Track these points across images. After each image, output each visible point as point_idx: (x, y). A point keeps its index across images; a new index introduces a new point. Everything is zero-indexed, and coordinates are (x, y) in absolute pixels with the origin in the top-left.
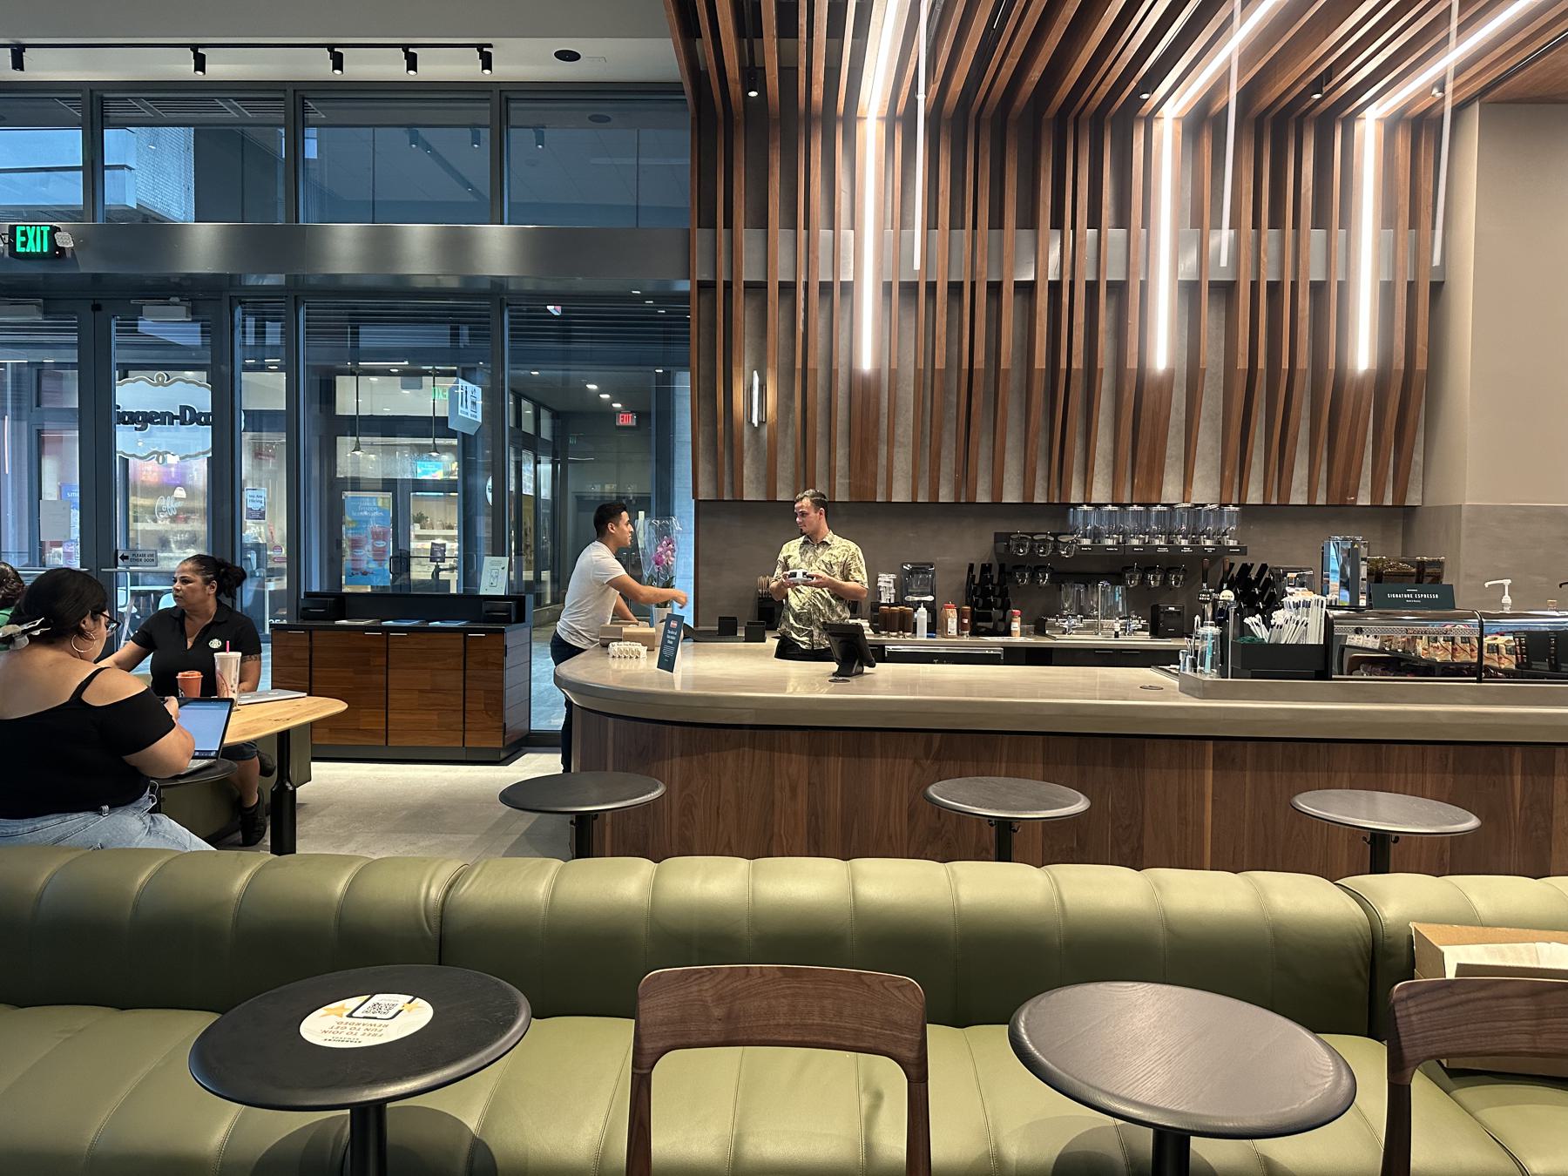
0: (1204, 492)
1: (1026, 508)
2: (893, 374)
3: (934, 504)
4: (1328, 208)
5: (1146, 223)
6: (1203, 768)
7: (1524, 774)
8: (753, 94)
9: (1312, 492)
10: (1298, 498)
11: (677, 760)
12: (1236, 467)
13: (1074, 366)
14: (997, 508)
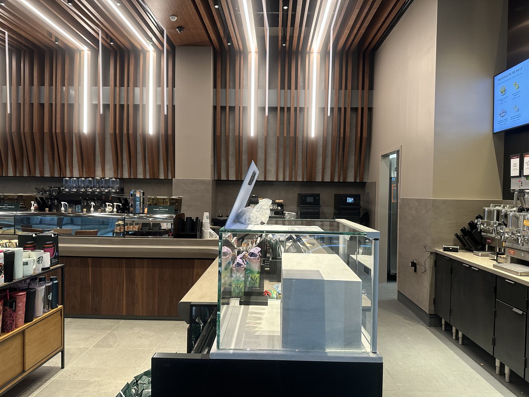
0: (109, 174)
1: (52, 179)
2: (266, 139)
3: (228, 180)
4: (138, 81)
5: (308, 89)
6: (89, 267)
7: (92, 267)
8: (229, 44)
9: (145, 174)
10: (140, 176)
11: (145, 269)
12: (118, 165)
13: (130, 132)
14: (42, 179)
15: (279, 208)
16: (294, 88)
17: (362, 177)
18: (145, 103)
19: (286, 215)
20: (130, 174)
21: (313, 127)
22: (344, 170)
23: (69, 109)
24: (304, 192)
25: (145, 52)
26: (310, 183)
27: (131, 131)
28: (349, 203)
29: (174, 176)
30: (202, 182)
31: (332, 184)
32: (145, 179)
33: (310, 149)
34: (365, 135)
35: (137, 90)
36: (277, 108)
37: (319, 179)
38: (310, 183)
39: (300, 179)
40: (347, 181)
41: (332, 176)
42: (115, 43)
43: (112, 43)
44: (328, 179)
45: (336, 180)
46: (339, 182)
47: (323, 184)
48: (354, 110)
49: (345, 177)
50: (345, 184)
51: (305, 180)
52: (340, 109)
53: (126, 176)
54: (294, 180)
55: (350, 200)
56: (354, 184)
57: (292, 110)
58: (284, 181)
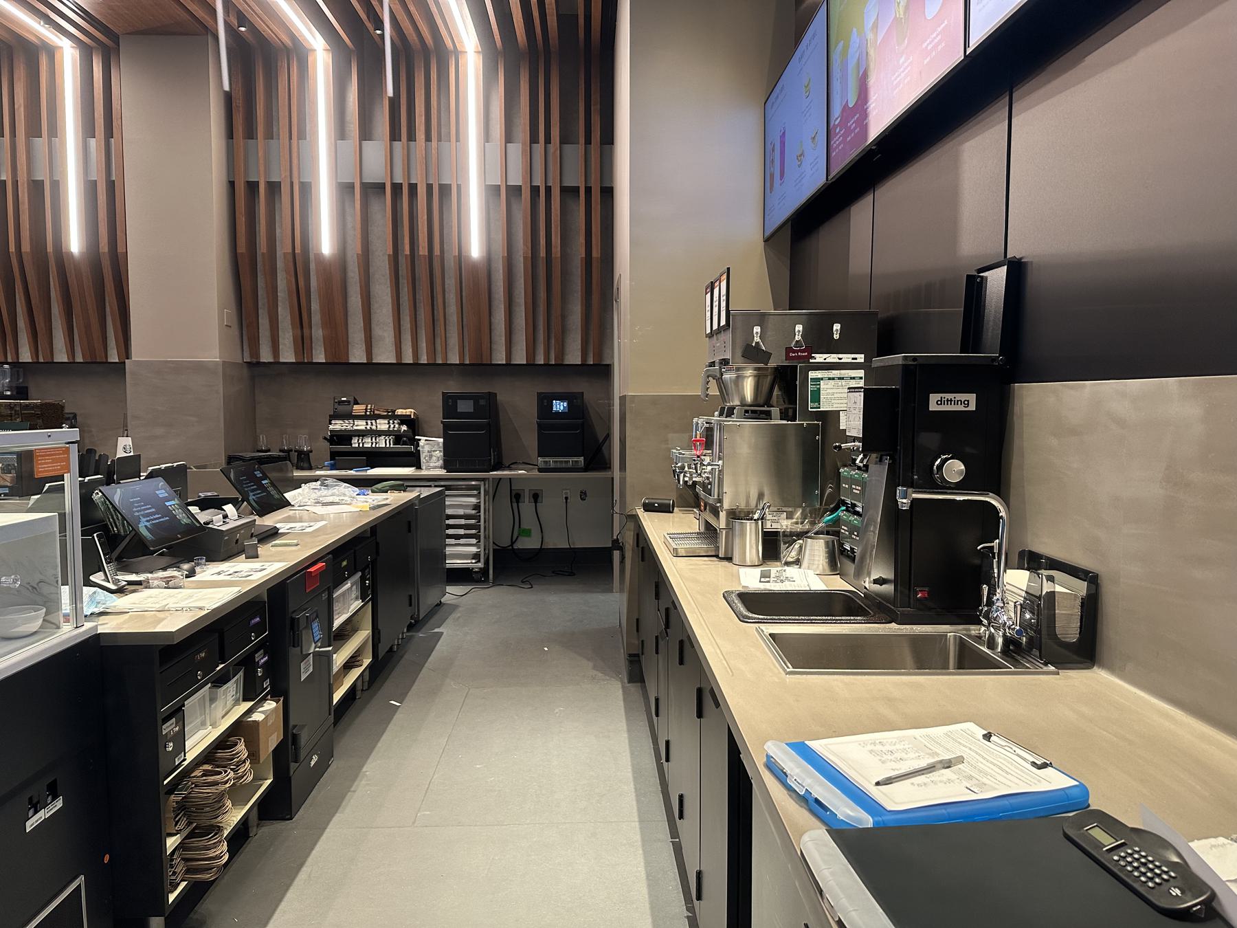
5: (458, 140)
9: (71, 351)
10: (61, 356)
15: (404, 428)
16: (423, 137)
17: (599, 353)
18: (41, 174)
19: (421, 443)
20: (36, 352)
21: (475, 233)
22: (558, 335)
23: (42, 194)
24: (453, 387)
25: (298, 53)
26: (480, 368)
27: (423, 250)
28: (557, 413)
29: (126, 350)
30: (199, 368)
31: (530, 368)
32: (416, 365)
33: (476, 284)
34: (596, 253)
35: (40, 143)
36: (382, 186)
37: (500, 358)
38: (480, 368)
39: (454, 359)
40: (494, 362)
41: (531, 351)
42: (253, 29)
43: (243, 29)
44: (520, 358)
45: (540, 360)
46: (546, 365)
47: (510, 369)
48: (569, 192)
49: (561, 352)
50: (559, 370)
51: (467, 362)
52: (535, 190)
53: (26, 356)
54: (440, 361)
55: (559, 406)
56: (582, 370)
57: (285, 189)
58: (508, 365)
